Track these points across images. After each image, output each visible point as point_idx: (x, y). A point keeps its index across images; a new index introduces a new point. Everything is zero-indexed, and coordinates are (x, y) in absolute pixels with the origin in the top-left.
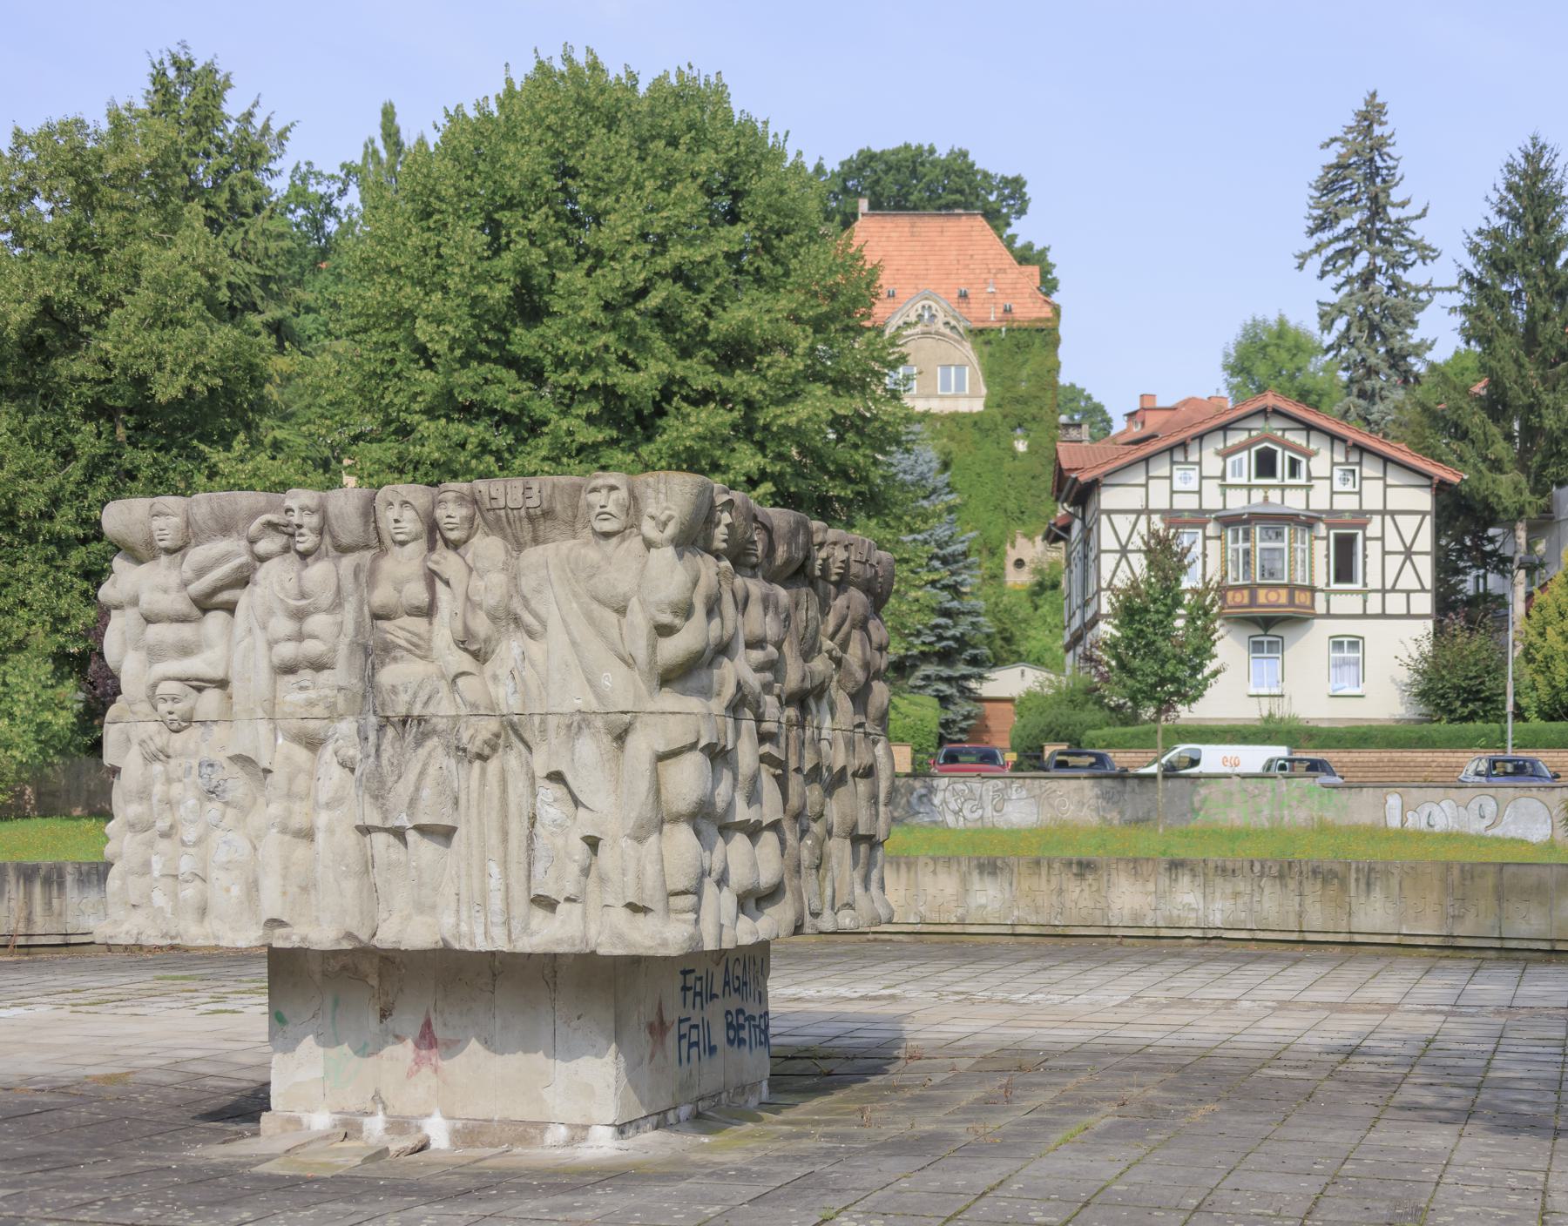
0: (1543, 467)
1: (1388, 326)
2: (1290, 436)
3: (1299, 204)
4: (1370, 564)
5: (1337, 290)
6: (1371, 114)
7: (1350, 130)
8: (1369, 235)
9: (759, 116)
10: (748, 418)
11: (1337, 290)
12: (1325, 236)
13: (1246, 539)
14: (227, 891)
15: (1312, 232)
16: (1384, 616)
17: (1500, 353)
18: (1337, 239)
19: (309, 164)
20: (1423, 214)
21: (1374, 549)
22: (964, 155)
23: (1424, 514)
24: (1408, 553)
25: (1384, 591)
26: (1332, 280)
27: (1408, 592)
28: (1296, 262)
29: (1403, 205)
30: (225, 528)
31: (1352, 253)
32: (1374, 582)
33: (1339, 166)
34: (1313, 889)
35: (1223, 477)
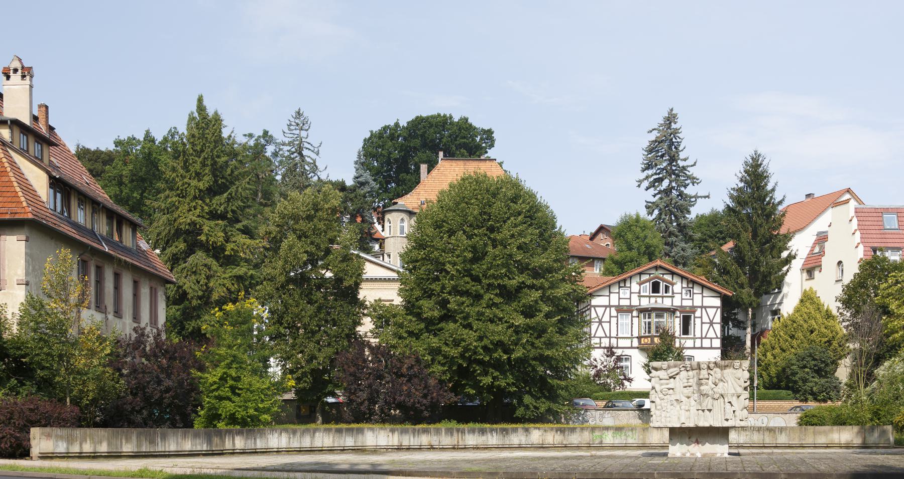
0: (760, 286)
1: (679, 214)
2: (666, 277)
3: (639, 158)
4: (697, 327)
5: (654, 196)
6: (671, 119)
7: (661, 125)
8: (670, 173)
9: (535, 190)
10: (544, 294)
11: (654, 196)
12: (650, 172)
13: (649, 318)
14: (692, 420)
15: (643, 171)
16: (702, 348)
17: (743, 240)
18: (656, 174)
19: (175, 128)
20: (694, 165)
21: (698, 321)
22: (467, 120)
23: (717, 307)
24: (711, 323)
25: (702, 338)
26: (652, 191)
27: (711, 339)
28: (637, 184)
29: (685, 160)
30: (675, 366)
31: (660, 180)
32: (698, 335)
33: (656, 141)
34: (767, 433)
35: (639, 293)
